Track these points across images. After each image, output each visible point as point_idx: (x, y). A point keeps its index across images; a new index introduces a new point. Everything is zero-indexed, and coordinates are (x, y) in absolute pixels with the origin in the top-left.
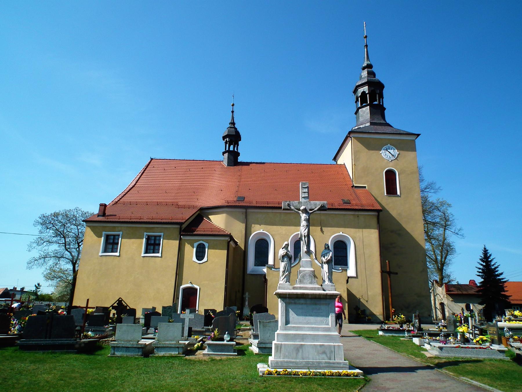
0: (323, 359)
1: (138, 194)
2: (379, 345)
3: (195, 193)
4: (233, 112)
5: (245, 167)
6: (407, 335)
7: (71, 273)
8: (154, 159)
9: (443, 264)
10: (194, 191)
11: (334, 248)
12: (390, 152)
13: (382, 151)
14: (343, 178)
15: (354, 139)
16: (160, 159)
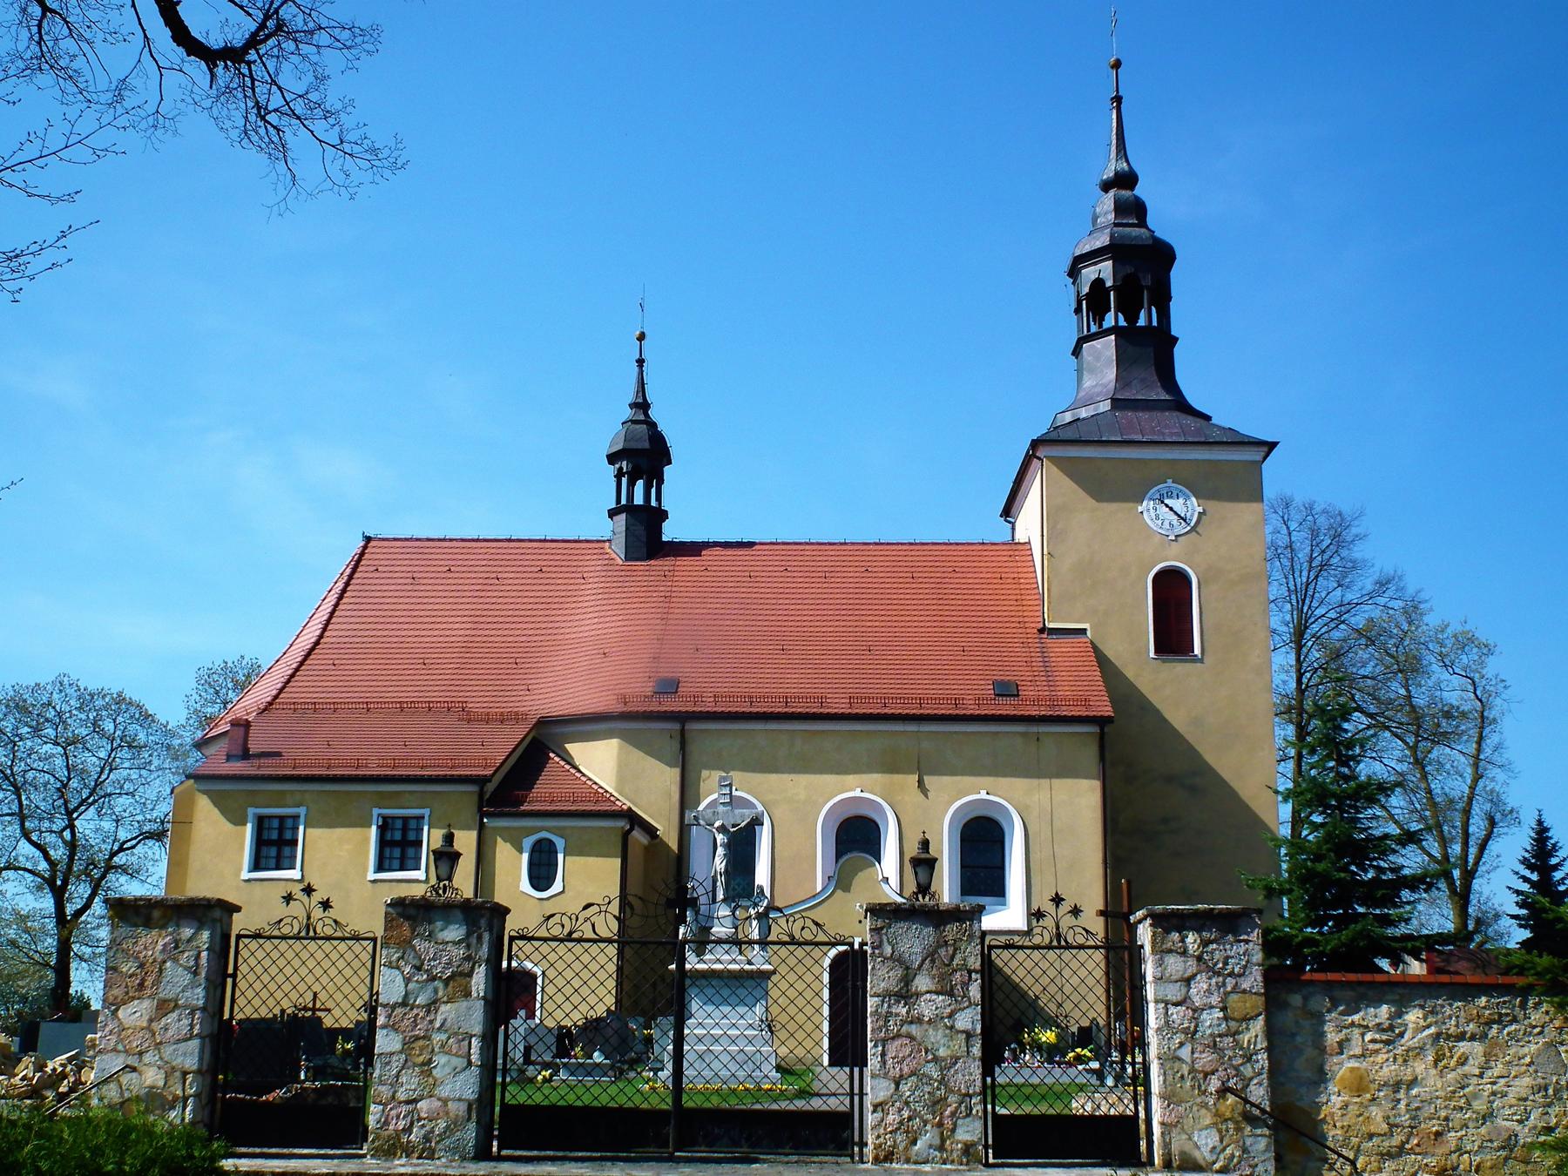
4: (640, 362)
5: (685, 562)
7: (51, 925)
9: (1469, 875)
10: (517, 655)
12: (1171, 509)
13: (1145, 503)
14: (1015, 597)
16: (395, 540)
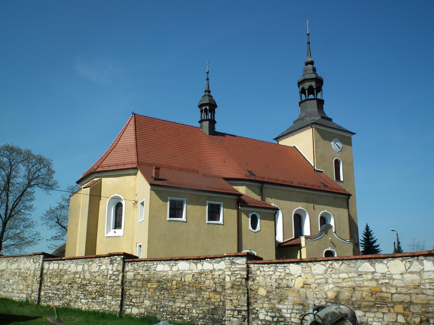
12: (337, 145)
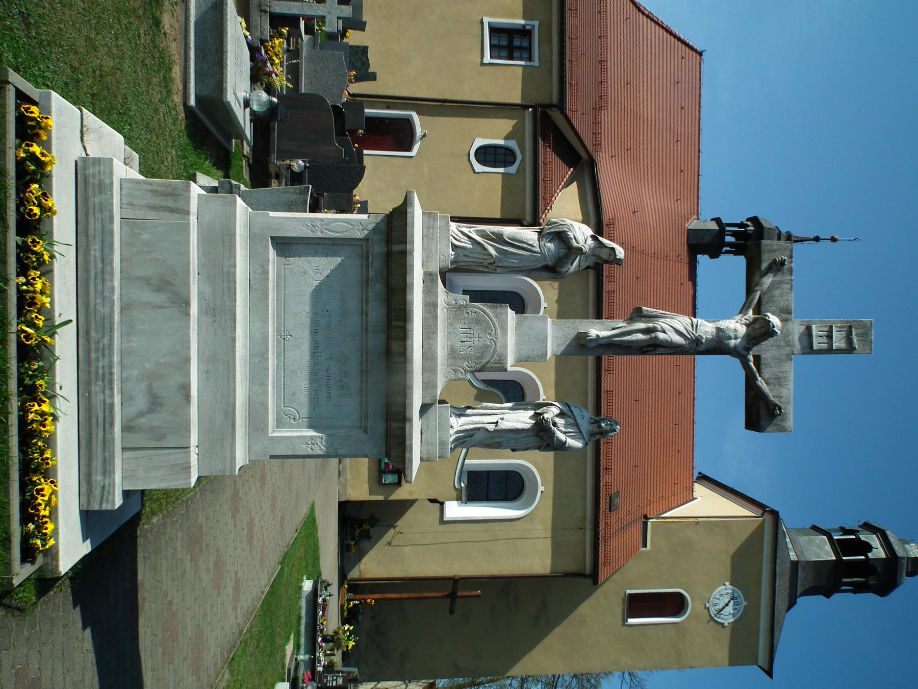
0: (127, 399)
1: (622, 19)
2: (262, 593)
3: (626, 152)
4: (817, 239)
6: (302, 660)
8: (700, 59)
11: (507, 471)
12: (727, 605)
15: (759, 523)
16: (700, 72)
